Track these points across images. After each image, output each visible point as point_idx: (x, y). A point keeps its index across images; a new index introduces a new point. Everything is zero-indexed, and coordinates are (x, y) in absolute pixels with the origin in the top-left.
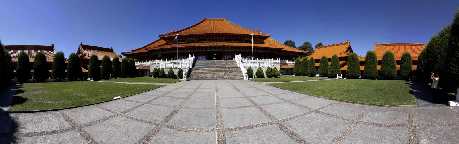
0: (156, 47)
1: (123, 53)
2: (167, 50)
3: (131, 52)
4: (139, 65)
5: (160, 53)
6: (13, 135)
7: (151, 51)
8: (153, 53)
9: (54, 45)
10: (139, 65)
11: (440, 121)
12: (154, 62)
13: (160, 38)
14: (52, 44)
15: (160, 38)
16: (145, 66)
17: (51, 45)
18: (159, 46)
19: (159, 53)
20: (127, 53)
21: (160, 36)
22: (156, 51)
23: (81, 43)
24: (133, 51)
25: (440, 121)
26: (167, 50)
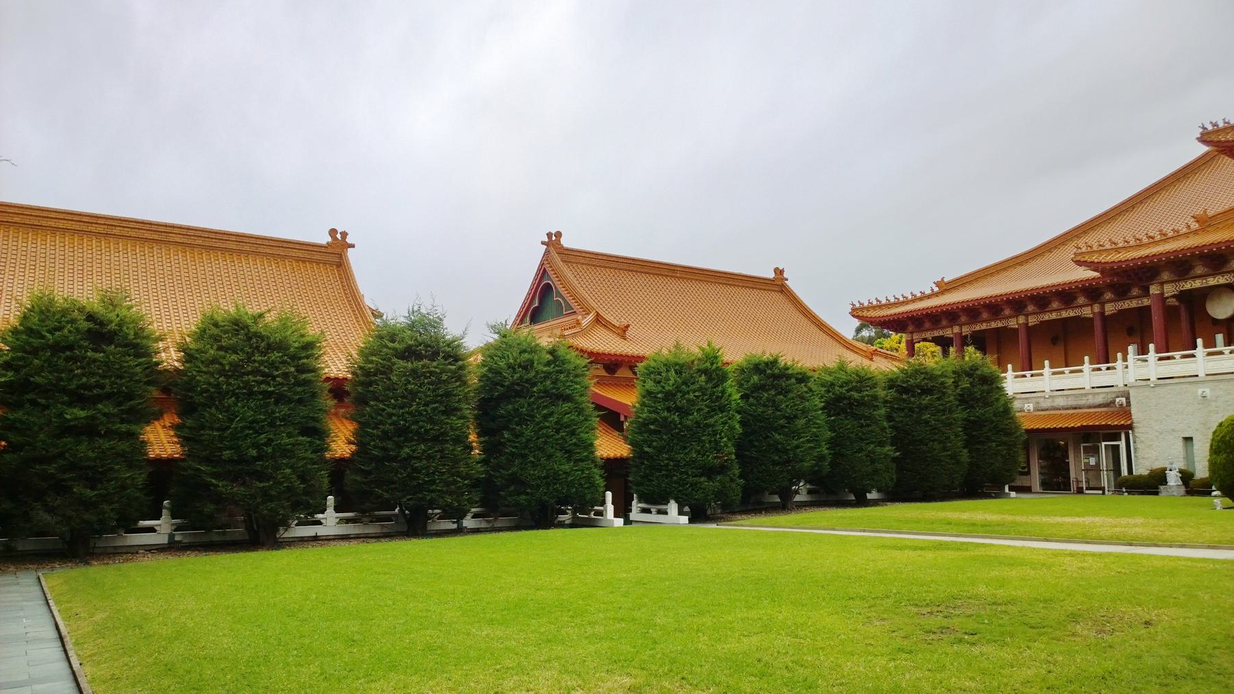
0: (1178, 236)
1: (862, 309)
2: (985, 315)
3: (933, 295)
4: (1039, 390)
5: (1222, 280)
6: (352, 419)
7: (1128, 277)
8: (1154, 290)
9: (349, 240)
10: (1039, 390)
11: (1137, 529)
12: (1178, 365)
13: (1204, 149)
14: (333, 232)
15: (1204, 149)
16: (1071, 402)
17: (325, 239)
18: (1205, 223)
19: (1212, 281)
20: (898, 304)
21: (1204, 138)
22: (1181, 264)
23: (559, 234)
24: (945, 287)
25: (1137, 529)
26: (985, 315)
